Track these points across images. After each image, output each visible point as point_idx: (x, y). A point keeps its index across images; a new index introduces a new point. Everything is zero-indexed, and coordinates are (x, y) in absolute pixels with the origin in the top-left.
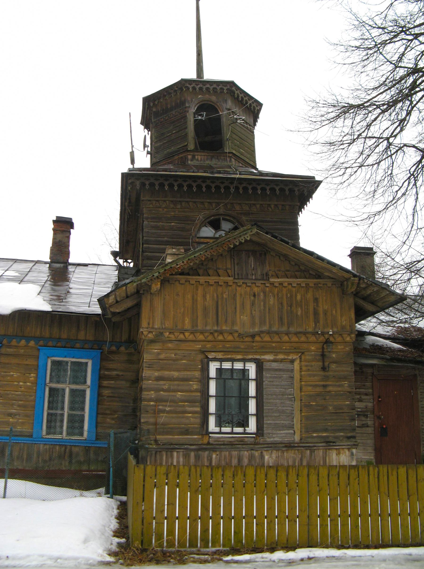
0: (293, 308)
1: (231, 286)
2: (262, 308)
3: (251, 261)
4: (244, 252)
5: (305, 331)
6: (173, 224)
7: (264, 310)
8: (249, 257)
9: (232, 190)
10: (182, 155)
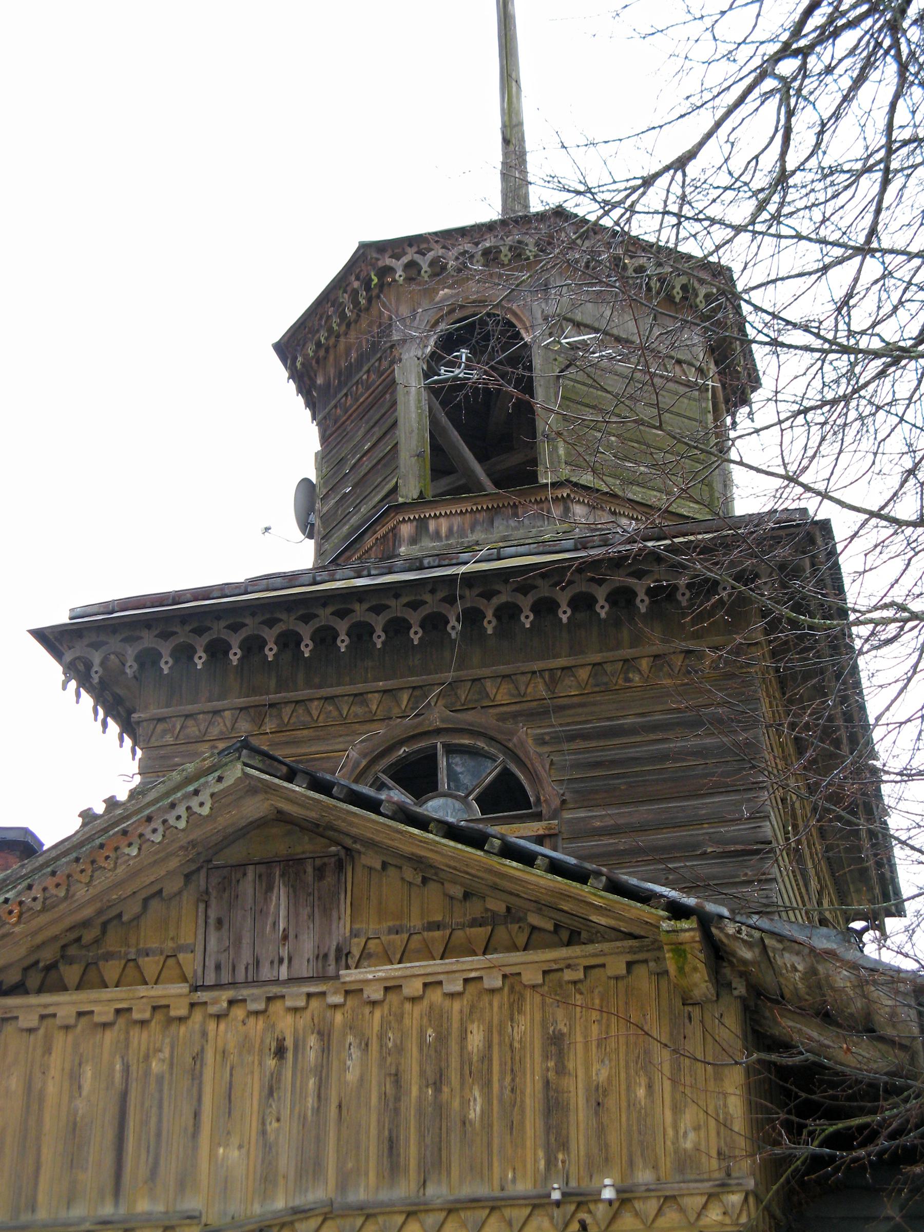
0: (446, 1089)
1: (181, 1020)
2: (311, 1102)
3: (278, 906)
4: (250, 870)
5: (497, 1193)
7: (317, 1111)
8: (270, 888)
9: (454, 628)
10: (384, 530)
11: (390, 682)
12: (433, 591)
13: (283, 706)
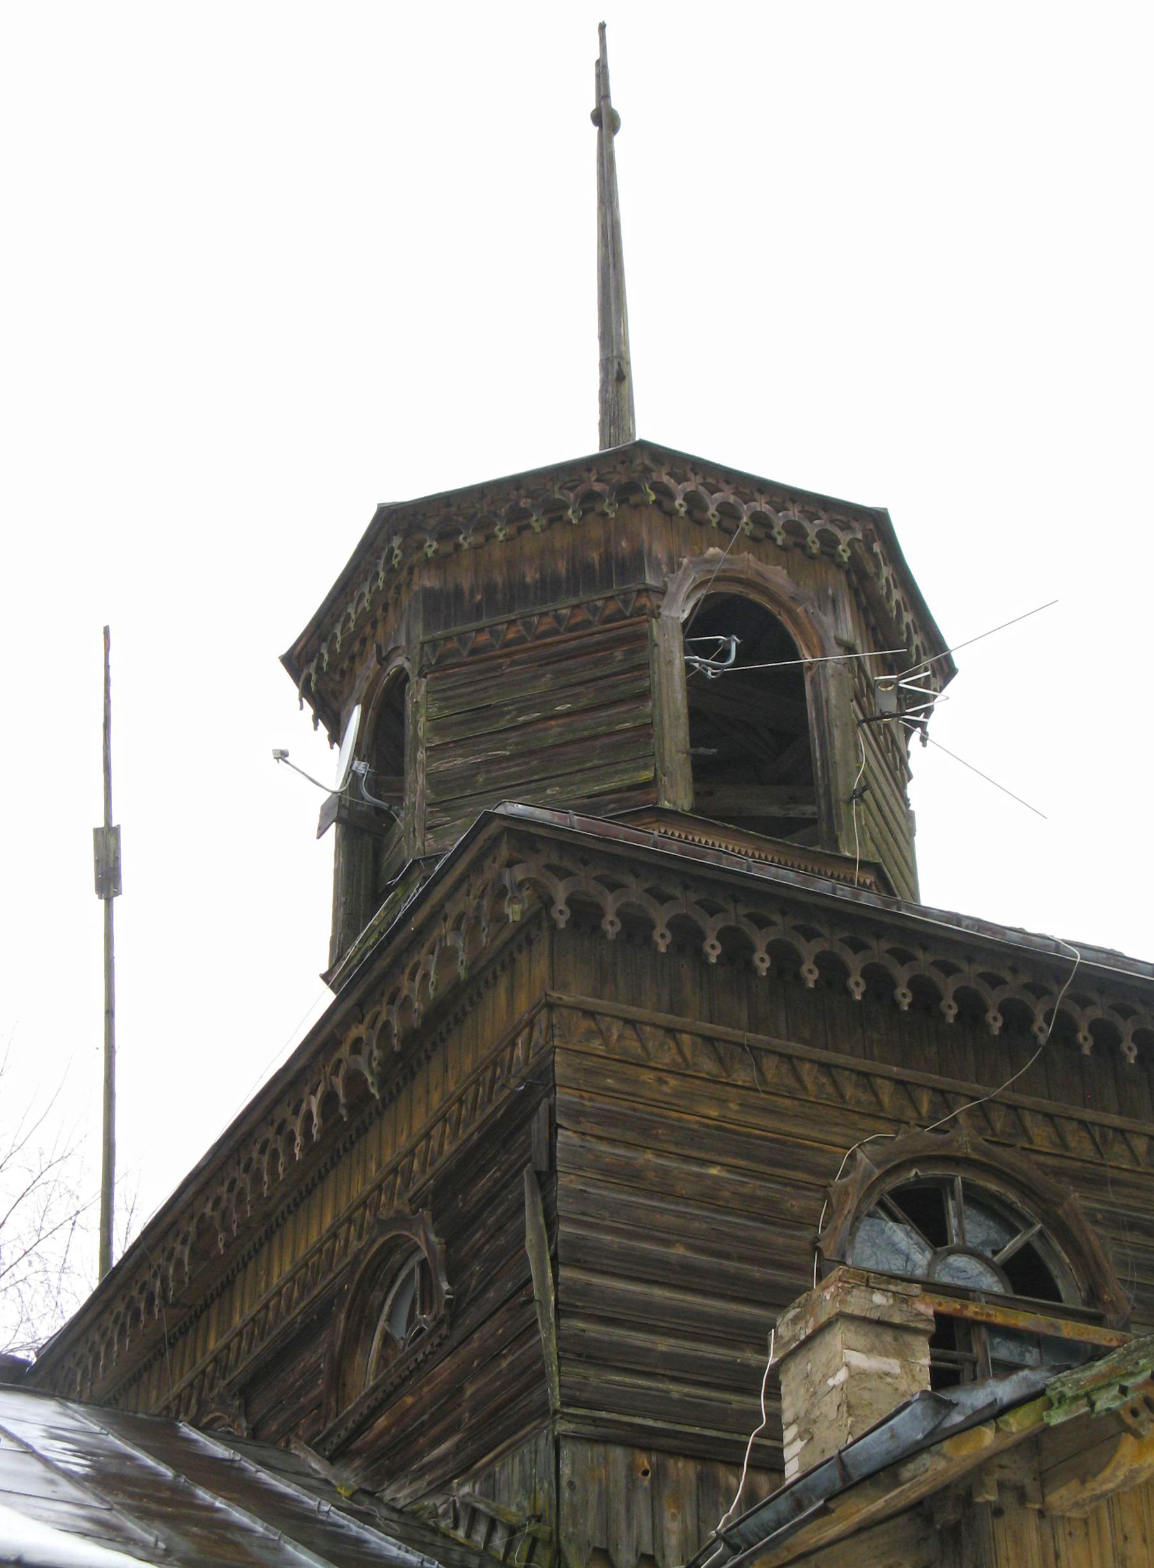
6: (714, 1171)
11: (907, 1071)
12: (1014, 970)
13: (763, 1053)
